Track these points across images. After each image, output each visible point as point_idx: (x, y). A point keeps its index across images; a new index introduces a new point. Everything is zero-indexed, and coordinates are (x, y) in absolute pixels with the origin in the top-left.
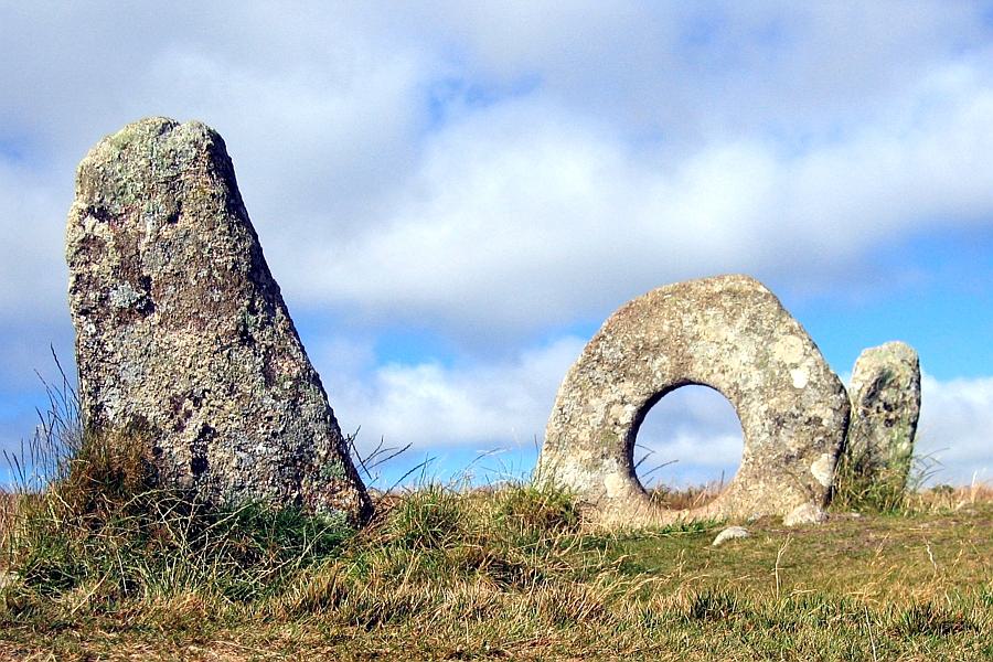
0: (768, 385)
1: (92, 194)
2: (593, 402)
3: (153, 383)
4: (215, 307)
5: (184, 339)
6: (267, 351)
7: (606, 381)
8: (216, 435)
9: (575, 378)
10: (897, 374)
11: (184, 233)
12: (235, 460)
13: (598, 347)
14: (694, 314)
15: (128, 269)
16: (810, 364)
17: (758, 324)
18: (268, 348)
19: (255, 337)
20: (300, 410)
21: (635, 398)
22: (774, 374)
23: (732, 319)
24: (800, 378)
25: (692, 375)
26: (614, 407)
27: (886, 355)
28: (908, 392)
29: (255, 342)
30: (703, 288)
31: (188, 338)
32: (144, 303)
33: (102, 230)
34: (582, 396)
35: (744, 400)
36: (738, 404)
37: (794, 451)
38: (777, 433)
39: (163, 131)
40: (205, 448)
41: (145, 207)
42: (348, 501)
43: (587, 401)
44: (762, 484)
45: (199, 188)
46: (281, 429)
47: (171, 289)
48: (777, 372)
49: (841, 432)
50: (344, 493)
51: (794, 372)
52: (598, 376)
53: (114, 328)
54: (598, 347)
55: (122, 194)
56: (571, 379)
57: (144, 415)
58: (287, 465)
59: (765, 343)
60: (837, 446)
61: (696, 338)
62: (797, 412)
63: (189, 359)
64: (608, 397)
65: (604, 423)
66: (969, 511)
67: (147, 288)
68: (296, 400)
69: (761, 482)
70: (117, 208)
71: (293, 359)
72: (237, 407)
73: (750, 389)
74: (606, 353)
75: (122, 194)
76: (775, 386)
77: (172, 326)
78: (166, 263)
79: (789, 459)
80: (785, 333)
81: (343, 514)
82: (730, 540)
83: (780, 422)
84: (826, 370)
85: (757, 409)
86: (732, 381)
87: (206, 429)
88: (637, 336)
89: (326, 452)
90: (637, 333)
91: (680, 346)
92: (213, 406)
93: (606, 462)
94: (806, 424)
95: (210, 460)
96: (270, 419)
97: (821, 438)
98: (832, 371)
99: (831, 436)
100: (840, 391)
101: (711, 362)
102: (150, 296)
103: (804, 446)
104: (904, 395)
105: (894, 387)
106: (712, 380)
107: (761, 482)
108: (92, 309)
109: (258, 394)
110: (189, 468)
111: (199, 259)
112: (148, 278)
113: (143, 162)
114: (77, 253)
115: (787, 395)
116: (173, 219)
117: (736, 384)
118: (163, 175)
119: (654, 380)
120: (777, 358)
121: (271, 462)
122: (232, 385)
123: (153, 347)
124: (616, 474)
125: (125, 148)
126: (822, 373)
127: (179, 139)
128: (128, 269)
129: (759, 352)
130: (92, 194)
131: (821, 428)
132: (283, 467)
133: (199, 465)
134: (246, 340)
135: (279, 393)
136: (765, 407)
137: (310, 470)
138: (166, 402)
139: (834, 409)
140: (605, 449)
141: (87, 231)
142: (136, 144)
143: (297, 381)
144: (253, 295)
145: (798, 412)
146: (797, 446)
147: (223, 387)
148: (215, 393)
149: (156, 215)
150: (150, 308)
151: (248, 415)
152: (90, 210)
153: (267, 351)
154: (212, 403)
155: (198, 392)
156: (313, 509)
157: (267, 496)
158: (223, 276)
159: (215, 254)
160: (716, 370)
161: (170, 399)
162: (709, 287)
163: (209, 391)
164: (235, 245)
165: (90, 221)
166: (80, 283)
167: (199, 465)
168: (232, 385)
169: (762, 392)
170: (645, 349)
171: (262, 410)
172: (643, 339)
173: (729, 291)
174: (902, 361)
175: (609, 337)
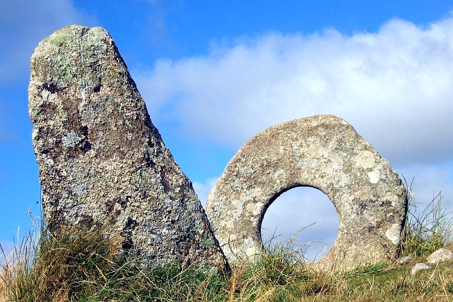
0: (353, 183)
1: (45, 75)
2: (234, 202)
3: (94, 194)
4: (129, 143)
5: (111, 165)
6: (162, 170)
7: (242, 188)
8: (137, 224)
11: (105, 97)
12: (150, 240)
13: (236, 166)
14: (300, 141)
15: (72, 123)
16: (380, 168)
17: (343, 145)
18: (162, 168)
19: (154, 161)
20: (186, 206)
21: (263, 198)
22: (357, 175)
23: (325, 143)
24: (374, 178)
25: (301, 180)
26: (249, 205)
29: (155, 164)
30: (305, 124)
31: (114, 164)
32: (84, 144)
33: (53, 98)
35: (338, 194)
36: (333, 197)
37: (374, 223)
38: (362, 213)
39: (83, 34)
40: (130, 233)
41: (80, 83)
42: (217, 261)
44: (354, 247)
45: (111, 69)
46: (177, 218)
47: (101, 134)
48: (359, 175)
49: (403, 209)
50: (214, 256)
51: (369, 174)
52: (237, 185)
53: (66, 161)
54: (236, 166)
55: (64, 75)
56: (218, 188)
57: (90, 215)
58: (181, 241)
59: (349, 157)
60: (402, 218)
61: (302, 156)
62: (374, 199)
63: (116, 178)
65: (242, 215)
67: (86, 134)
68: (183, 199)
69: (353, 245)
70: (62, 84)
72: (149, 206)
73: (341, 187)
74: (242, 170)
75: (64, 75)
76: (358, 183)
77: (104, 157)
78: (96, 118)
79: (371, 229)
80: (362, 149)
83: (363, 206)
84: (391, 171)
85: (347, 200)
86: (328, 183)
87: (130, 221)
88: (262, 158)
89: (202, 231)
90: (263, 156)
91: (291, 162)
92: (134, 206)
93: (246, 241)
95: (134, 241)
96: (170, 212)
98: (394, 171)
99: (397, 212)
100: (400, 184)
103: (380, 220)
106: (315, 183)
107: (353, 245)
108: (51, 149)
109: (161, 197)
112: (86, 128)
113: (74, 54)
114: (38, 114)
115: (367, 189)
116: (97, 90)
119: (275, 185)
120: (358, 165)
121: (172, 239)
122: (145, 193)
123: (92, 172)
124: (254, 248)
125: (61, 45)
126: (388, 173)
127: (94, 39)
128: (72, 123)
129: (345, 162)
130: (45, 75)
131: (391, 208)
132: (179, 242)
133: (127, 245)
134: (150, 164)
135: (173, 195)
136: (352, 197)
137: (194, 243)
138: (103, 206)
140: (245, 232)
141: (44, 99)
142: (68, 42)
143: (182, 187)
144: (150, 135)
145: (375, 199)
146: (376, 220)
147: (139, 194)
148: (134, 198)
149: (87, 87)
150: (88, 147)
151: (156, 210)
153: (162, 170)
154: (133, 204)
155: (123, 198)
157: (167, 261)
159: (125, 110)
161: (106, 203)
162: (309, 123)
163: (130, 197)
164: (137, 104)
165: (45, 93)
166: (43, 133)
167: (127, 245)
168: (145, 193)
169: (349, 187)
170: (268, 166)
171: (164, 207)
172: (266, 159)
173: (323, 125)
175: (243, 160)
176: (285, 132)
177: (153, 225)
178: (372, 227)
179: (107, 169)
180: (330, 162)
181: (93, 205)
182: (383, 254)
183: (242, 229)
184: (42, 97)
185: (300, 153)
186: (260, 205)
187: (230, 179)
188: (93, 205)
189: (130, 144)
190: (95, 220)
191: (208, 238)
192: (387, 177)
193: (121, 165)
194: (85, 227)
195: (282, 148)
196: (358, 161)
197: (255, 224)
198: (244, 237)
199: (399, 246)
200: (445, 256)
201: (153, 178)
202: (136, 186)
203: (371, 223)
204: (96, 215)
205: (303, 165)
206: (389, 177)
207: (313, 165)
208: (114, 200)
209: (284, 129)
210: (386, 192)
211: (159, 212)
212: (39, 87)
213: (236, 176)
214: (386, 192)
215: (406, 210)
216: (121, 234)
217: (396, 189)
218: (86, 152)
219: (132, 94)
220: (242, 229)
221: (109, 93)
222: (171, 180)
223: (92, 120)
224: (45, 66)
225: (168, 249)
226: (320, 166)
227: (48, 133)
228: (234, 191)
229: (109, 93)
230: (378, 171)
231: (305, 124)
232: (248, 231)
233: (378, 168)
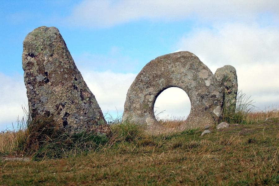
0: (198, 86)
1: (29, 50)
2: (140, 95)
4: (66, 79)
5: (58, 89)
8: (69, 115)
9: (133, 87)
10: (229, 76)
11: (55, 59)
12: (75, 121)
13: (141, 77)
17: (193, 66)
18: (81, 90)
19: (77, 87)
22: (199, 82)
24: (208, 83)
26: (147, 96)
27: (225, 70)
28: (233, 82)
30: (174, 56)
32: (46, 79)
33: (32, 60)
34: (136, 93)
35: (190, 91)
41: (44, 53)
43: (138, 95)
44: (198, 118)
45: (58, 46)
46: (87, 112)
53: (38, 87)
54: (141, 77)
57: (49, 111)
59: (196, 72)
60: (221, 104)
61: (173, 72)
63: (60, 94)
64: (145, 93)
65: (144, 101)
66: (270, 121)
67: (47, 75)
68: (90, 103)
70: (36, 54)
71: (88, 92)
72: (75, 106)
73: (192, 87)
75: (37, 49)
79: (206, 109)
80: (202, 69)
81: (104, 134)
82: (206, 134)
83: (202, 97)
86: (186, 85)
93: (146, 114)
94: (211, 97)
96: (84, 109)
97: (216, 101)
99: (219, 101)
101: (178, 79)
102: (48, 77)
103: (210, 104)
104: (232, 83)
105: (229, 81)
110: (62, 124)
111: (60, 66)
112: (47, 73)
113: (42, 40)
114: (26, 67)
115: (204, 89)
116: (52, 56)
117: (187, 86)
118: (48, 43)
122: (73, 101)
124: (149, 118)
126: (215, 81)
127: (51, 33)
128: (41, 70)
136: (197, 93)
139: (220, 92)
141: (28, 60)
142: (39, 35)
145: (208, 94)
146: (208, 104)
147: (70, 101)
148: (68, 103)
149: (47, 55)
150: (48, 81)
152: (29, 55)
155: (63, 103)
156: (97, 133)
158: (67, 71)
160: (180, 82)
161: (56, 106)
162: (176, 55)
163: (66, 103)
165: (29, 58)
167: (65, 123)
169: (196, 88)
170: (157, 77)
172: (155, 73)
173: (183, 57)
174: (231, 72)
175: (144, 74)
176: (165, 60)
177: (77, 115)
178: (207, 108)
179: (56, 90)
180: (187, 75)
181: (50, 106)
182: (212, 121)
183: (144, 108)
184: (27, 59)
185: (172, 70)
186: (152, 96)
187: (138, 83)
188: (50, 106)
189: (66, 80)
190: (51, 113)
191: (101, 120)
192: (214, 83)
193: (62, 89)
194: (46, 116)
195: (163, 68)
196: (200, 75)
197: (150, 106)
198: (145, 112)
199: (220, 117)
200: (224, 126)
201: (77, 94)
202: (69, 98)
203: (206, 106)
204: (52, 111)
205: (173, 76)
206: (215, 83)
207: (178, 77)
208: (59, 104)
209: (164, 58)
210: (214, 90)
211: (79, 109)
212: (26, 55)
213: (141, 81)
214: (214, 90)
215: (224, 99)
216: (63, 119)
217: (219, 89)
218: (47, 83)
219: (68, 57)
220: (144, 108)
221: (57, 57)
222: (85, 95)
223: (50, 69)
224: (29, 46)
225: (83, 125)
226: (182, 77)
227: (30, 75)
228: (140, 89)
229: (57, 57)
230: (210, 80)
231: (174, 56)
232: (147, 109)
233: (210, 78)
